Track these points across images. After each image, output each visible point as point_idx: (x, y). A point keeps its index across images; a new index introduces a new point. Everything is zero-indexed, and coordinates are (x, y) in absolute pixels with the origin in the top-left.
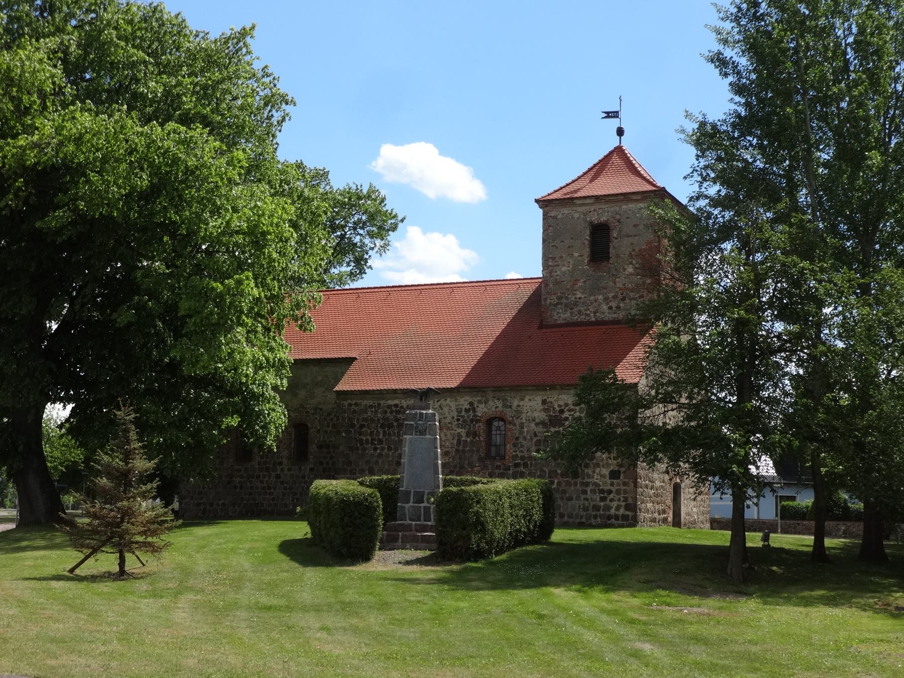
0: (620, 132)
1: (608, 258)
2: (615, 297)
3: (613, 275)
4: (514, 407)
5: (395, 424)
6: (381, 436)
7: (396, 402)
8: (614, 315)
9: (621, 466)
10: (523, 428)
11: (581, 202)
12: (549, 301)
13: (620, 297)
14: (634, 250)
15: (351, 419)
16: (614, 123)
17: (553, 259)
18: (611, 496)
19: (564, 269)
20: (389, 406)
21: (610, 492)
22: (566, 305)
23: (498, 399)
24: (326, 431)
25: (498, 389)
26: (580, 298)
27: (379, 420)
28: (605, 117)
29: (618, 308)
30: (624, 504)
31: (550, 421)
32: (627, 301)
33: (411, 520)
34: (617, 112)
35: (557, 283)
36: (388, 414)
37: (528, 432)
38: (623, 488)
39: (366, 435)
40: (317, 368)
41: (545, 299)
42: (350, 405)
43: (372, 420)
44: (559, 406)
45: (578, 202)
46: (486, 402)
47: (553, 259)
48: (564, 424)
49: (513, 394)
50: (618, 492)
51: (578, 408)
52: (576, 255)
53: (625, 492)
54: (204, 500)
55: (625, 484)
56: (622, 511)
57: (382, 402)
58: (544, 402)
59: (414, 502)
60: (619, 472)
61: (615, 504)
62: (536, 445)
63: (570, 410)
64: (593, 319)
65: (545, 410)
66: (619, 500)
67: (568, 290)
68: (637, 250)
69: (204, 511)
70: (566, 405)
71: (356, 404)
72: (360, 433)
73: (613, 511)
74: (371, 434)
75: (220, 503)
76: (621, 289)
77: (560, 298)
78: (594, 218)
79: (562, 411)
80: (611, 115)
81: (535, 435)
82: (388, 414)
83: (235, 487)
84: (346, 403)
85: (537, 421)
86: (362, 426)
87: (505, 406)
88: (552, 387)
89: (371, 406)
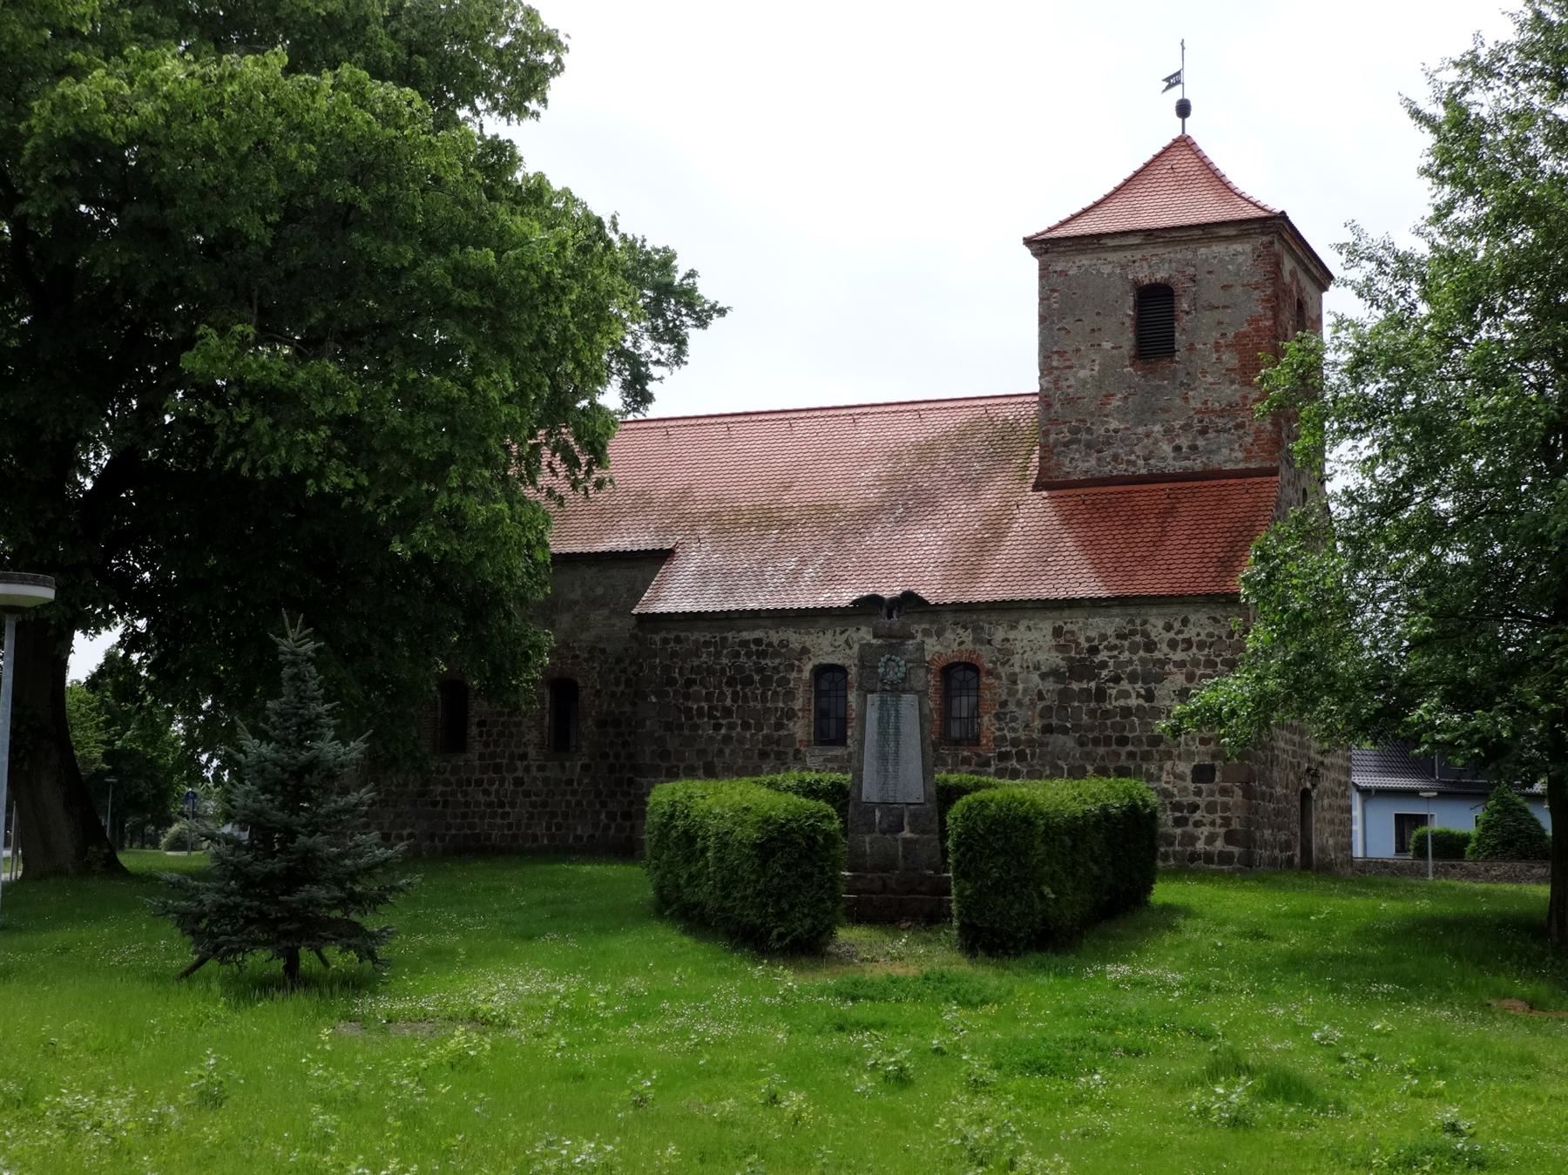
0: (1183, 109)
1: (1171, 352)
2: (1186, 428)
3: (1182, 384)
5: (757, 678)
6: (728, 702)
10: (1015, 682)
13: (1197, 426)
15: (667, 669)
17: (1061, 354)
19: (1082, 374)
20: (744, 643)
22: (1089, 445)
24: (613, 694)
27: (723, 671)
29: (1193, 448)
35: (1070, 401)
36: (743, 659)
37: (1025, 690)
39: (698, 700)
42: (665, 641)
43: (711, 671)
52: (1107, 345)
57: (730, 635)
58: (1057, 632)
71: (678, 640)
72: (687, 697)
75: (405, 833)
78: (1144, 275)
81: (1041, 696)
82: (743, 659)
83: (435, 804)
84: (657, 638)
86: (689, 683)
89: (707, 644)
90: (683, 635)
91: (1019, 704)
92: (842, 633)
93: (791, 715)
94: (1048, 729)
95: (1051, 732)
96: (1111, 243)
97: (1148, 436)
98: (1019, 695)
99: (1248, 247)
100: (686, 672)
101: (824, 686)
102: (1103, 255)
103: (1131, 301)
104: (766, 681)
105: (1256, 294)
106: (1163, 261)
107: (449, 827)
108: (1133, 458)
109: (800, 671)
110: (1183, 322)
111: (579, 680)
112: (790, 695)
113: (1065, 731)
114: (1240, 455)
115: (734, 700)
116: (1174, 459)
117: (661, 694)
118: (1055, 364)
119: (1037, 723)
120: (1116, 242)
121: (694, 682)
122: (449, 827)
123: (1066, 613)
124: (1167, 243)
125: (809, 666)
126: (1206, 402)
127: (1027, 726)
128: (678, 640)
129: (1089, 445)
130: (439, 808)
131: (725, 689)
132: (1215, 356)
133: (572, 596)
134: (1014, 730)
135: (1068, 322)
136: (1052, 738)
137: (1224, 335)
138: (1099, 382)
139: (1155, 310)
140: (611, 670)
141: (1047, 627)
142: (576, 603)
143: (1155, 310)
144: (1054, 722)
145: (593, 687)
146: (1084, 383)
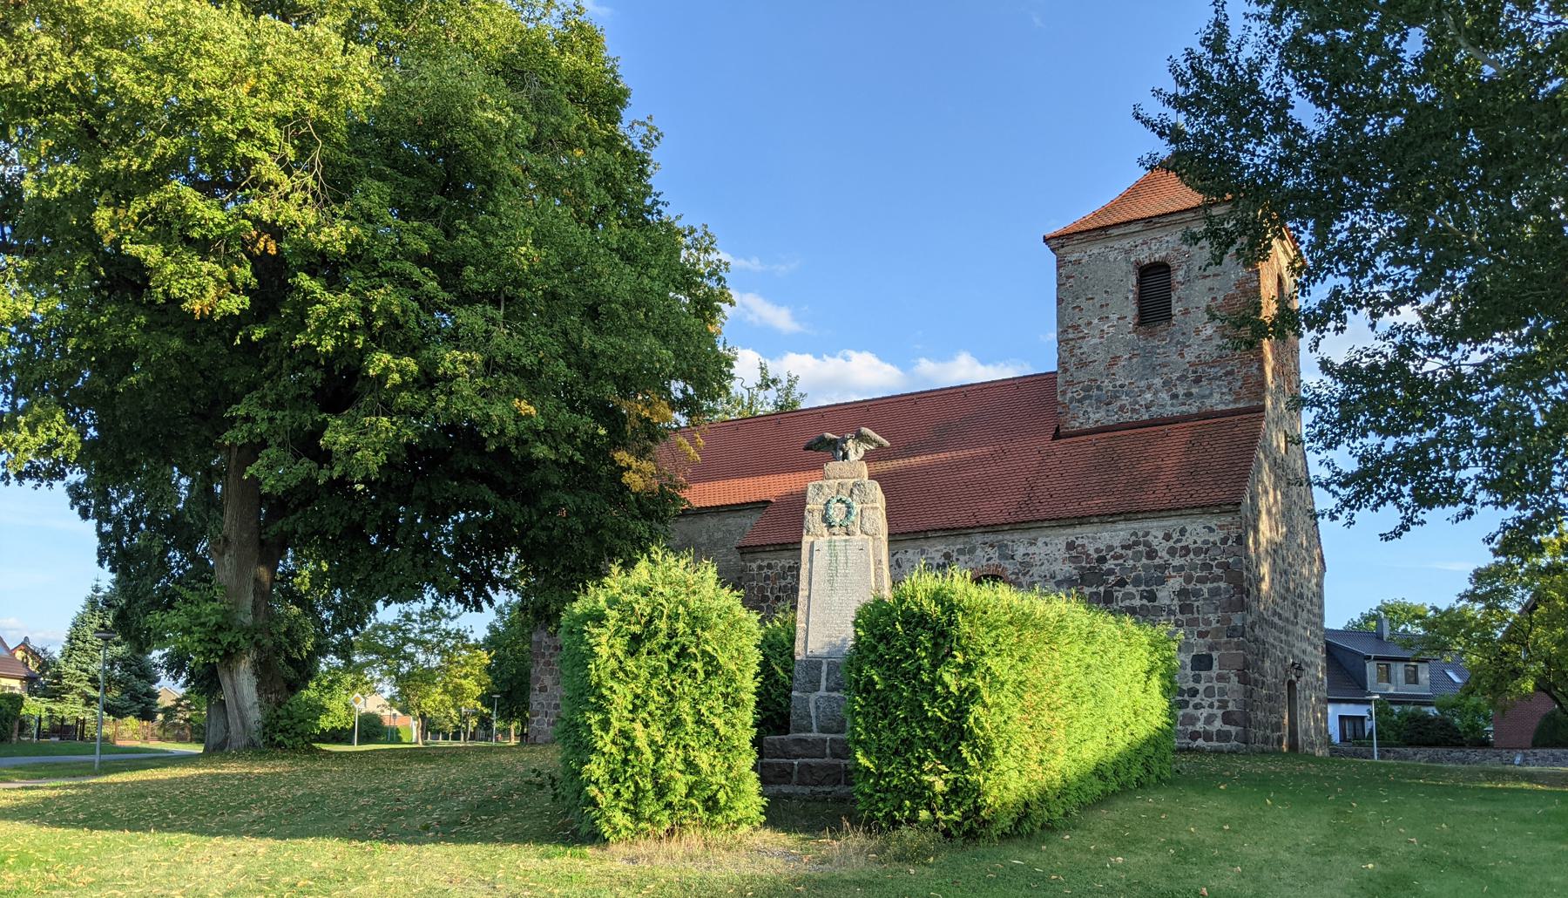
4: (1018, 558)
8: (1184, 408)
9: (1211, 648)
11: (1121, 231)
13: (1191, 376)
14: (1214, 299)
18: (1197, 700)
21: (1194, 693)
22: (1099, 400)
23: (992, 546)
25: (993, 528)
26: (1122, 386)
29: (1189, 395)
30: (1220, 712)
31: (1082, 577)
32: (1204, 382)
33: (823, 730)
38: (1217, 685)
40: (716, 520)
41: (1064, 393)
42: (760, 568)
44: (1097, 550)
45: (1115, 232)
46: (972, 551)
47: (1076, 328)
48: (1105, 582)
49: (1016, 536)
50: (1209, 692)
51: (1130, 553)
53: (1222, 692)
55: (1220, 678)
56: (1218, 724)
58: (1071, 546)
59: (828, 690)
60: (1210, 657)
61: (1205, 712)
63: (1115, 558)
64: (1146, 417)
65: (1074, 559)
66: (1211, 706)
67: (1101, 374)
68: (1220, 299)
70: (1110, 548)
71: (769, 566)
73: (1200, 726)
76: (1191, 364)
77: (1087, 389)
78: (1145, 256)
79: (1102, 560)
84: (754, 566)
85: (1059, 578)
87: (1003, 556)
88: (1082, 520)
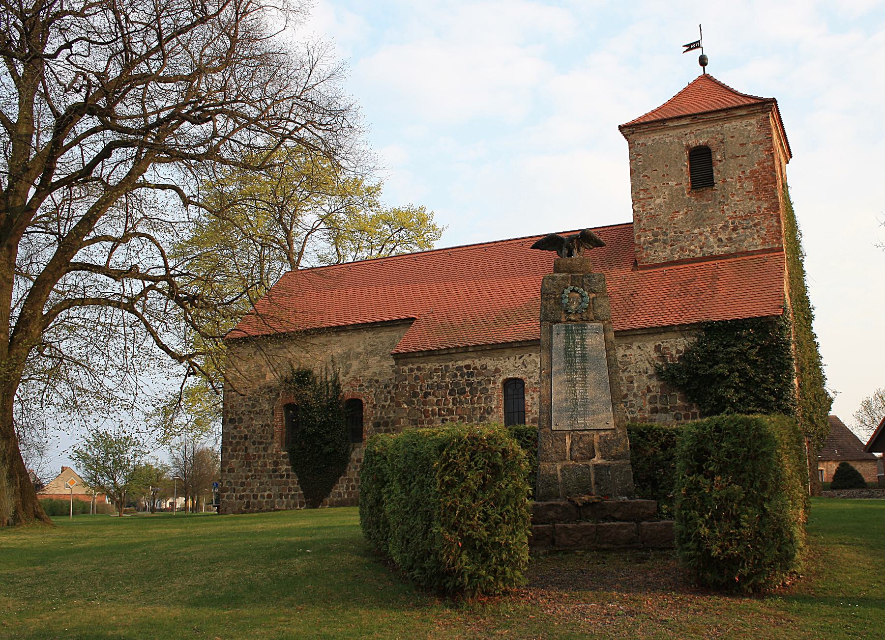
0: (703, 61)
1: (712, 184)
2: (725, 227)
3: (720, 202)
5: (468, 389)
6: (451, 406)
7: (468, 362)
10: (632, 382)
12: (643, 239)
13: (731, 226)
15: (412, 387)
16: (697, 53)
17: (645, 190)
19: (658, 201)
20: (459, 369)
22: (665, 242)
24: (384, 406)
27: (447, 385)
28: (687, 50)
29: (730, 239)
34: (699, 41)
35: (653, 217)
36: (459, 378)
37: (638, 387)
39: (432, 405)
41: (639, 237)
42: (411, 370)
43: (439, 387)
52: (672, 183)
54: (247, 493)
57: (450, 364)
58: (658, 349)
62: (650, 403)
69: (248, 506)
71: (419, 369)
72: (425, 403)
74: (438, 403)
75: (266, 494)
78: (693, 142)
80: (690, 47)
81: (649, 390)
82: (459, 378)
83: (282, 476)
84: (406, 368)
86: (426, 395)
89: (436, 370)
90: (422, 366)
91: (635, 395)
92: (520, 358)
93: (489, 411)
94: (655, 411)
95: (657, 412)
96: (671, 124)
97: (701, 234)
98: (635, 390)
99: (753, 121)
100: (424, 388)
101: (510, 391)
102: (667, 132)
103: (686, 156)
104: (473, 391)
105: (761, 148)
106: (703, 133)
107: (290, 490)
108: (692, 247)
109: (494, 383)
110: (718, 167)
111: (363, 399)
112: (489, 398)
113: (665, 411)
114: (759, 241)
115: (454, 404)
116: (718, 246)
117: (410, 403)
118: (641, 196)
119: (648, 407)
120: (675, 124)
121: (429, 394)
122: (290, 490)
123: (663, 336)
124: (705, 122)
125: (501, 380)
126: (735, 212)
127: (641, 409)
128: (419, 369)
129: (665, 242)
130: (284, 479)
131: (448, 397)
132: (738, 184)
133: (359, 350)
134: (633, 412)
135: (648, 172)
136: (657, 416)
137: (743, 172)
138: (669, 205)
139: (701, 164)
140: (382, 392)
141: (650, 347)
142: (360, 354)
143: (701, 164)
144: (659, 406)
145: (372, 403)
146: (660, 206)
